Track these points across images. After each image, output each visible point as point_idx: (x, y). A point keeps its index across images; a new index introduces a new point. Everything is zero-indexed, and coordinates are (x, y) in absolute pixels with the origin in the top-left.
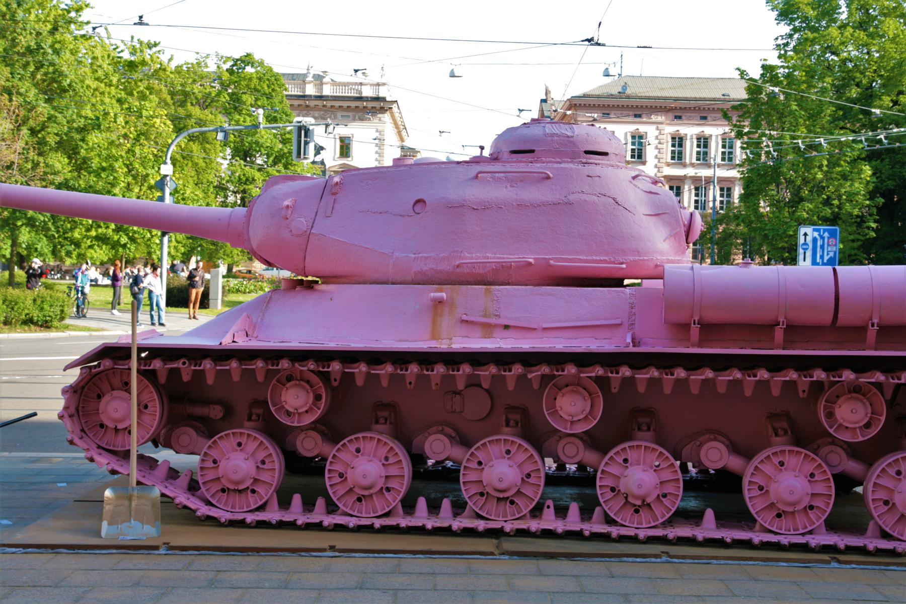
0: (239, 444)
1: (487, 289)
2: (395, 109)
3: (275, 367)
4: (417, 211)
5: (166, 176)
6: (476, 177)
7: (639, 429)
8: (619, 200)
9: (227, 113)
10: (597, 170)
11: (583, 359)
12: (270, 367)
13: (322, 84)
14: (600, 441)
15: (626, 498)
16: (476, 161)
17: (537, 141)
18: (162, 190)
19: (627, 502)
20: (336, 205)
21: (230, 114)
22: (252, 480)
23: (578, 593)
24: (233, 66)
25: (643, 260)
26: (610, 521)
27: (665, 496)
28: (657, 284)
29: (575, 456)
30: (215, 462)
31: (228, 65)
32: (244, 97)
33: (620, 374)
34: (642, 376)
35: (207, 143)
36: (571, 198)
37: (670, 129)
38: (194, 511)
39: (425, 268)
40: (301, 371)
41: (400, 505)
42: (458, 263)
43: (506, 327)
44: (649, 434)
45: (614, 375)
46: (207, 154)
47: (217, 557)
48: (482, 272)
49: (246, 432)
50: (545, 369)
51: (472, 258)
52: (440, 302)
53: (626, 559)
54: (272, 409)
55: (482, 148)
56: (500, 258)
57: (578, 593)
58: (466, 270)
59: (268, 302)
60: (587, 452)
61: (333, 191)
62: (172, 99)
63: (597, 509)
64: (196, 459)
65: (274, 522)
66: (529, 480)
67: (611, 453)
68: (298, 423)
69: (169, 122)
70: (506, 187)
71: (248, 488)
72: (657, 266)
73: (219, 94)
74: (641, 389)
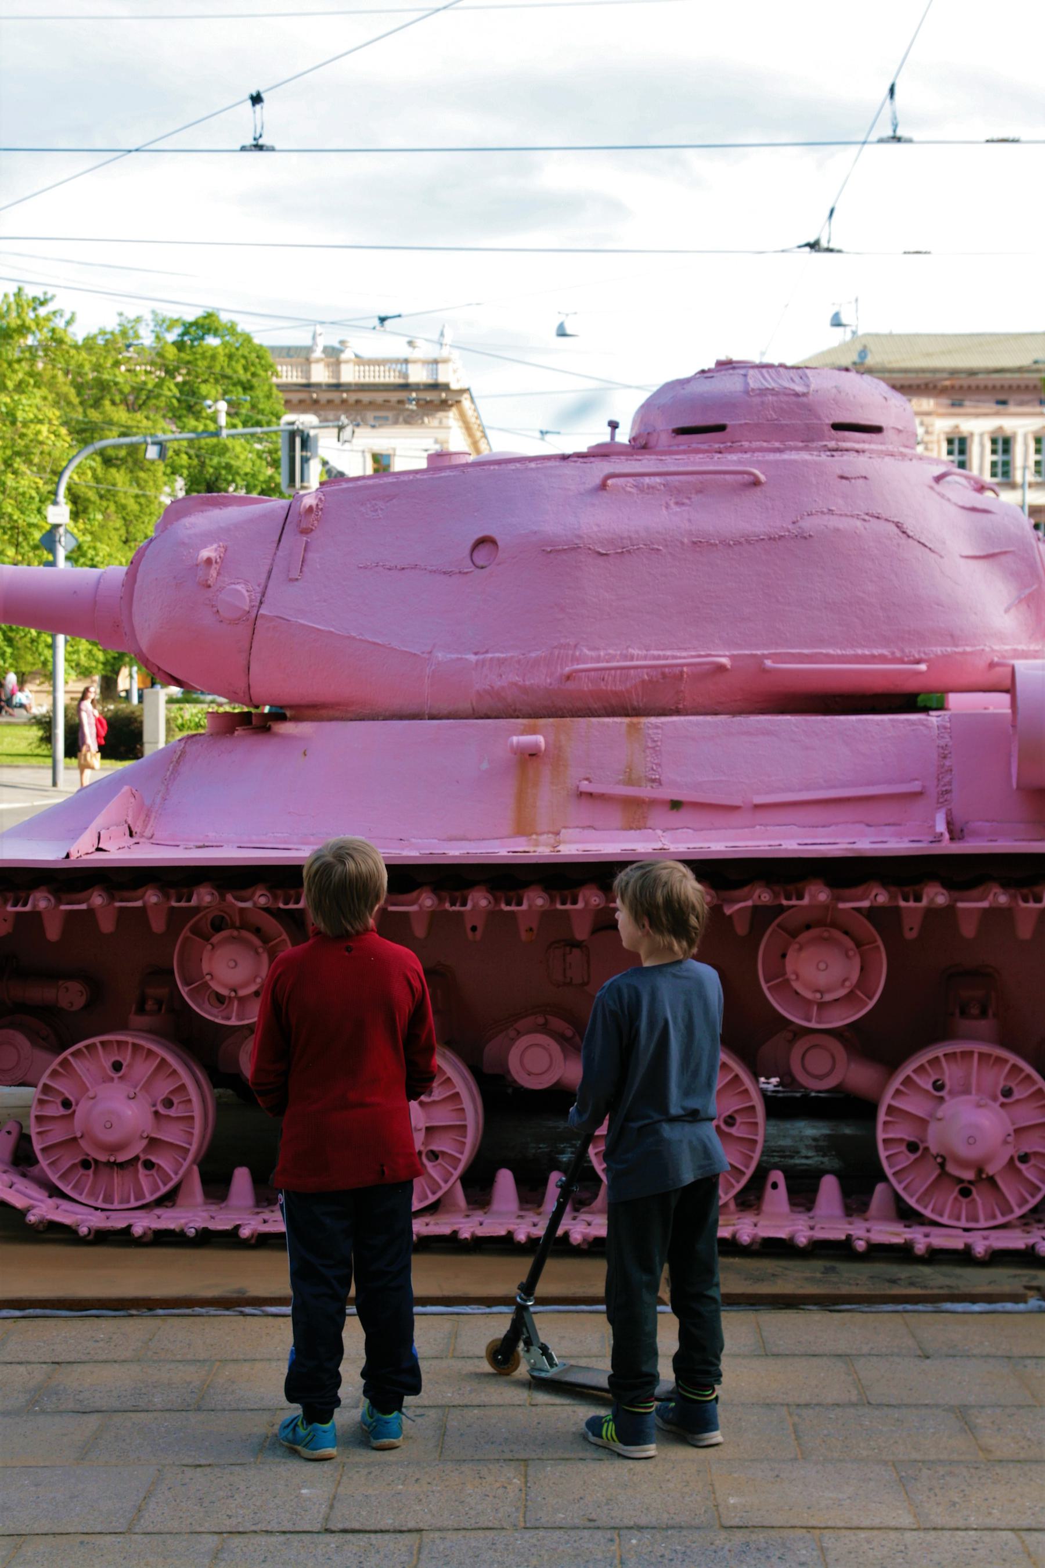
0: (117, 1066)
1: (631, 726)
2: (466, 403)
3: (183, 904)
4: (481, 563)
5: (56, 527)
6: (603, 486)
7: (964, 1013)
8: (909, 526)
9: (177, 418)
10: (858, 464)
11: (845, 872)
12: (174, 904)
13: (338, 363)
14: (885, 1040)
15: (942, 1165)
16: (601, 452)
17: (728, 404)
18: (52, 550)
19: (944, 1174)
20: (310, 555)
21: (180, 418)
22: (145, 1142)
23: (854, 1405)
24: (183, 334)
25: (964, 653)
26: (906, 1215)
27: (1024, 1158)
28: (998, 703)
29: (827, 1075)
30: (66, 1104)
31: (171, 337)
32: (204, 389)
33: (924, 903)
34: (971, 905)
35: (142, 469)
36: (808, 524)
37: (943, 425)
38: (22, 1213)
39: (498, 684)
40: (242, 910)
41: (459, 1185)
42: (567, 670)
43: (676, 805)
44: (983, 1025)
45: (911, 904)
46: (141, 488)
47: (61, 1322)
48: (620, 687)
49: (129, 1039)
50: (763, 896)
51: (598, 660)
52: (532, 754)
53: (948, 1306)
54: (184, 991)
55: (614, 425)
56: (658, 658)
57: (854, 1405)
58: (586, 686)
59: (178, 762)
60: (853, 1066)
61: (304, 525)
62: (79, 394)
63: (880, 1188)
64: (27, 1094)
65: (191, 1233)
66: (733, 1131)
67: (908, 1069)
68: (240, 1017)
69: (63, 431)
70: (667, 507)
71: (137, 1158)
72: (992, 665)
73: (160, 385)
74: (968, 930)
